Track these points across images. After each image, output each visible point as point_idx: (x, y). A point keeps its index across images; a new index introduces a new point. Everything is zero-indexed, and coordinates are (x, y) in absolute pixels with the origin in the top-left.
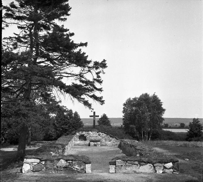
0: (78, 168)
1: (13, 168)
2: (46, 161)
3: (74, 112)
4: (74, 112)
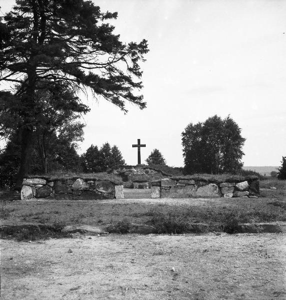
0: (104, 191)
2: (55, 181)
3: (112, 146)
4: (112, 146)
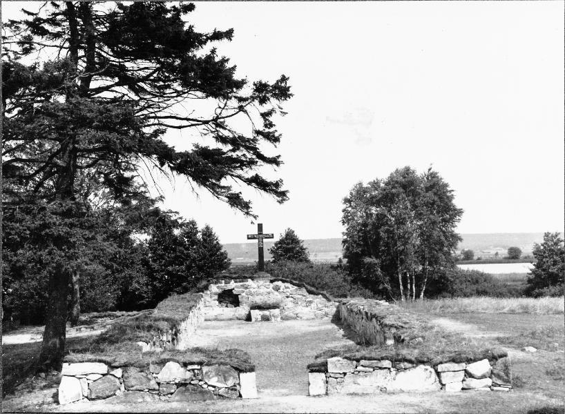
4: (201, 227)
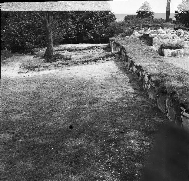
1: (36, 93)
